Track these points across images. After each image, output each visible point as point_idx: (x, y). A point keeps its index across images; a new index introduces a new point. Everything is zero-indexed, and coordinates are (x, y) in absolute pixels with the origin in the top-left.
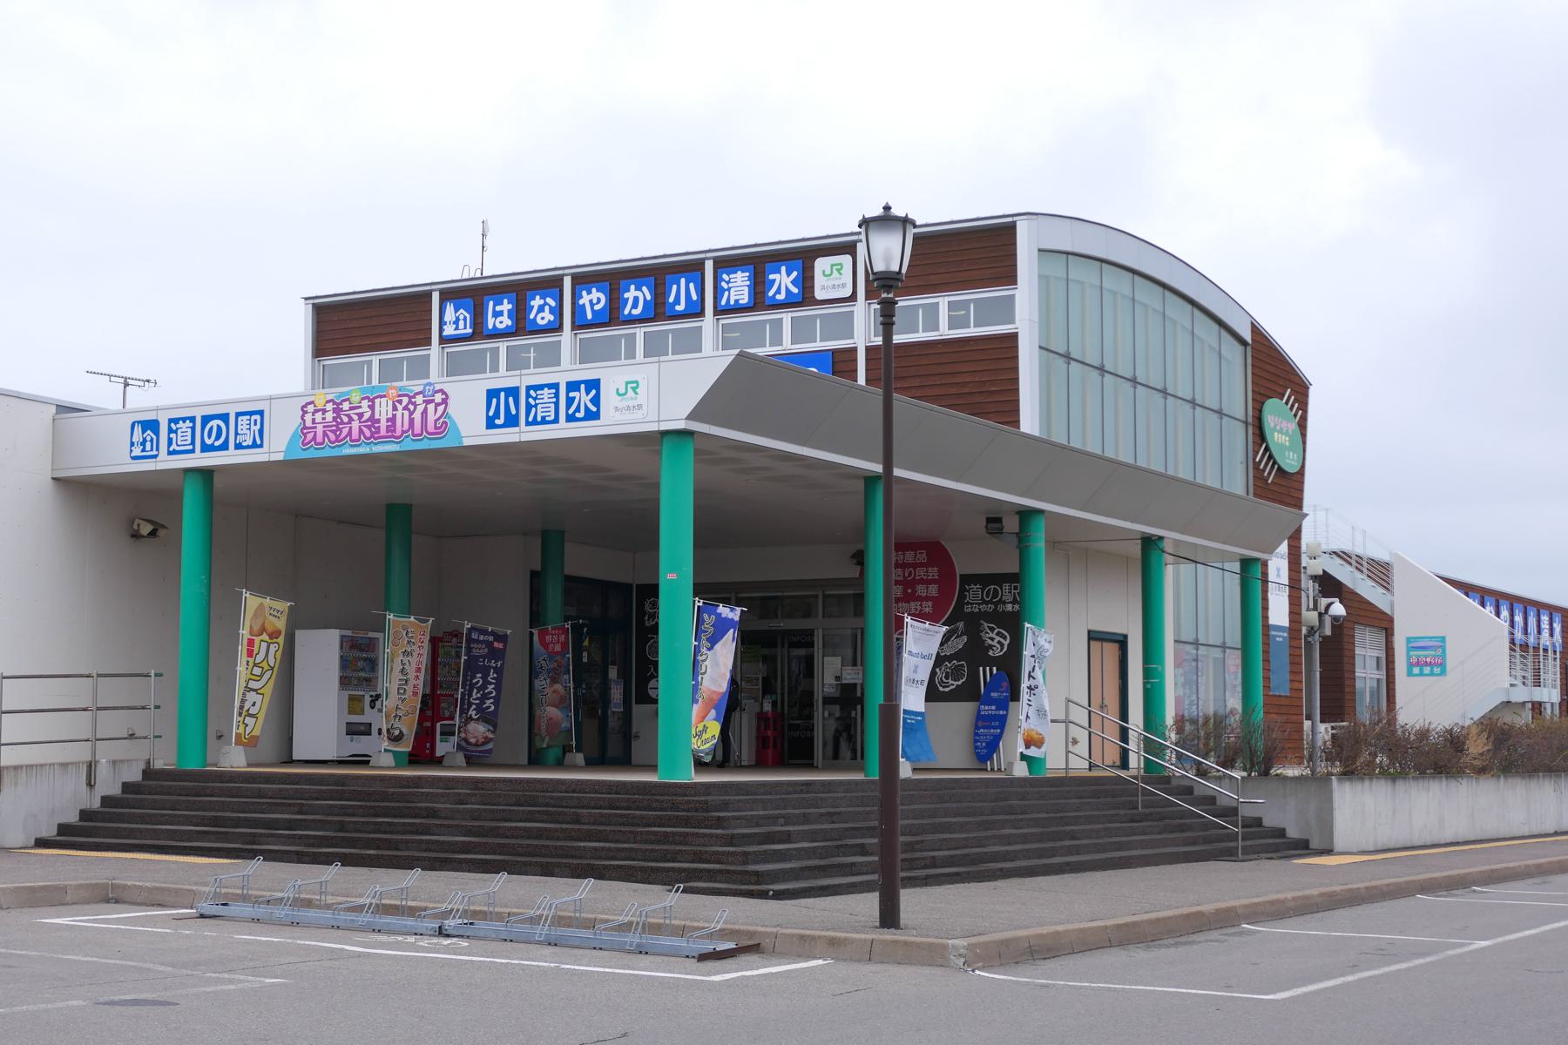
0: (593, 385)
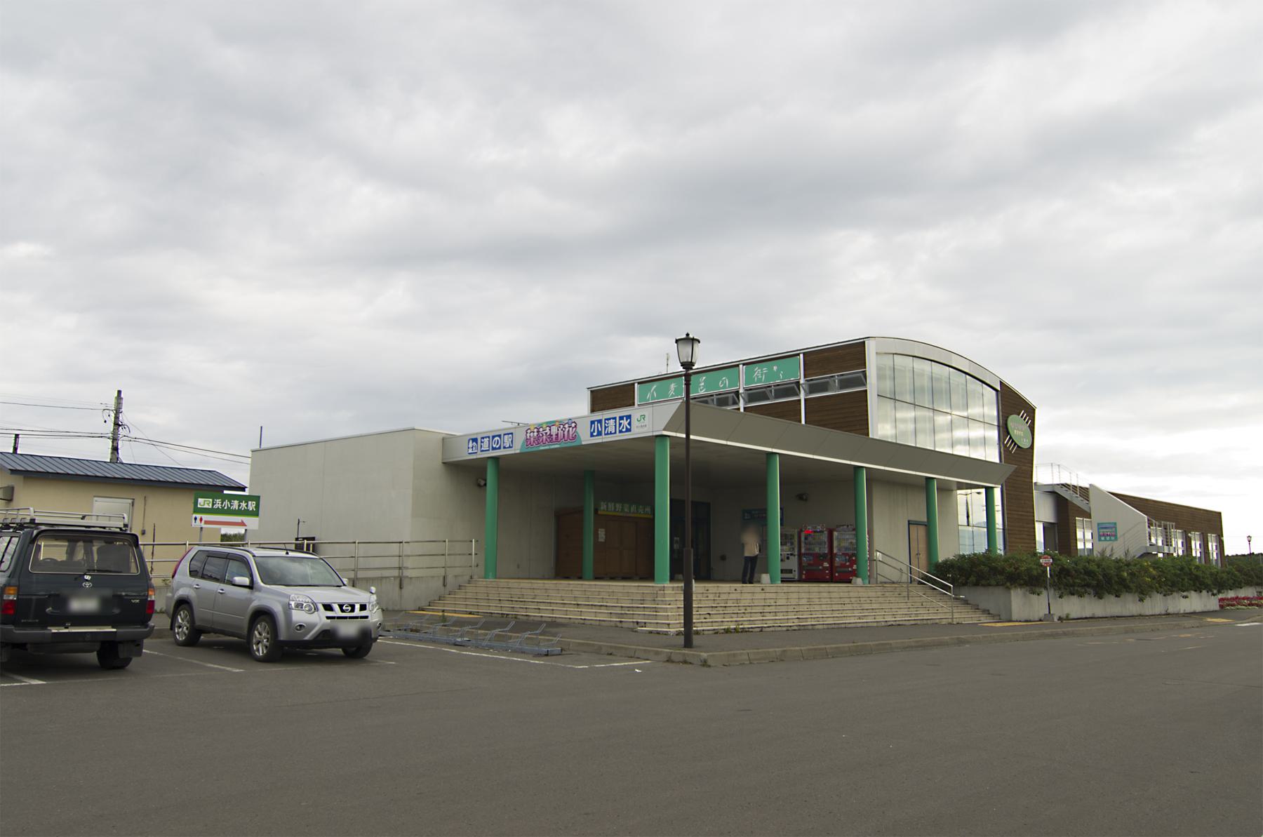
0: (629, 417)
